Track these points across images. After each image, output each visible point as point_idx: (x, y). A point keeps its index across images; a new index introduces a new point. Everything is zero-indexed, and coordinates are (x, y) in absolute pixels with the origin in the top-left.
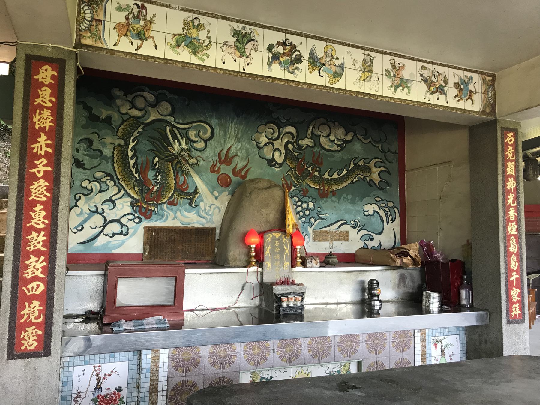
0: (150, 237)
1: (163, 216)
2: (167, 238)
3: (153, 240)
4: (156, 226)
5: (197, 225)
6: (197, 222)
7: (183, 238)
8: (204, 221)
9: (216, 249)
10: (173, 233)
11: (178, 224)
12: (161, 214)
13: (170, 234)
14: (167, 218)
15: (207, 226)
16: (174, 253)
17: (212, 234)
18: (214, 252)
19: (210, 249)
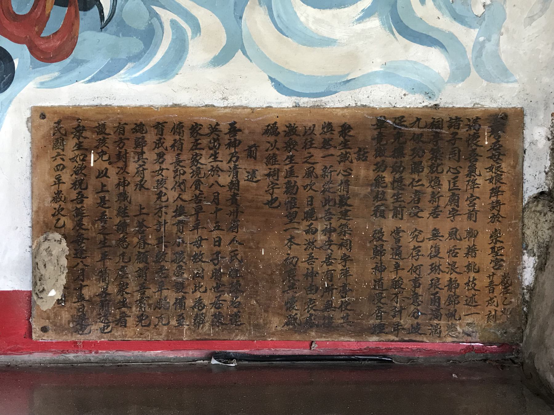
0: (67, 177)
1: (150, 36)
2: (181, 185)
3: (90, 200)
4: (104, 110)
5: (384, 97)
6: (389, 74)
7: (291, 188)
8: (435, 61)
9: (529, 262)
10: (224, 153)
11: (247, 90)
12: (142, 26)
13: (205, 161)
14: (180, 50)
15: (465, 96)
16: (236, 289)
17: (498, 152)
18: (510, 281)
19: (484, 258)
